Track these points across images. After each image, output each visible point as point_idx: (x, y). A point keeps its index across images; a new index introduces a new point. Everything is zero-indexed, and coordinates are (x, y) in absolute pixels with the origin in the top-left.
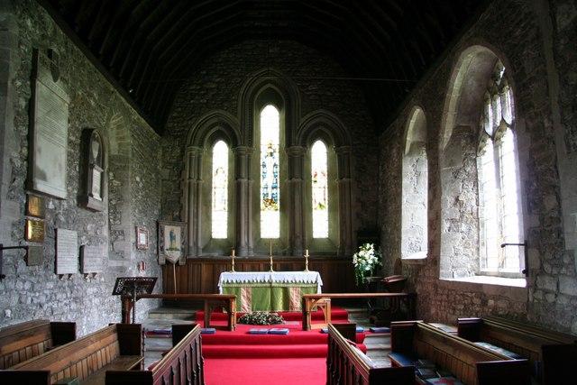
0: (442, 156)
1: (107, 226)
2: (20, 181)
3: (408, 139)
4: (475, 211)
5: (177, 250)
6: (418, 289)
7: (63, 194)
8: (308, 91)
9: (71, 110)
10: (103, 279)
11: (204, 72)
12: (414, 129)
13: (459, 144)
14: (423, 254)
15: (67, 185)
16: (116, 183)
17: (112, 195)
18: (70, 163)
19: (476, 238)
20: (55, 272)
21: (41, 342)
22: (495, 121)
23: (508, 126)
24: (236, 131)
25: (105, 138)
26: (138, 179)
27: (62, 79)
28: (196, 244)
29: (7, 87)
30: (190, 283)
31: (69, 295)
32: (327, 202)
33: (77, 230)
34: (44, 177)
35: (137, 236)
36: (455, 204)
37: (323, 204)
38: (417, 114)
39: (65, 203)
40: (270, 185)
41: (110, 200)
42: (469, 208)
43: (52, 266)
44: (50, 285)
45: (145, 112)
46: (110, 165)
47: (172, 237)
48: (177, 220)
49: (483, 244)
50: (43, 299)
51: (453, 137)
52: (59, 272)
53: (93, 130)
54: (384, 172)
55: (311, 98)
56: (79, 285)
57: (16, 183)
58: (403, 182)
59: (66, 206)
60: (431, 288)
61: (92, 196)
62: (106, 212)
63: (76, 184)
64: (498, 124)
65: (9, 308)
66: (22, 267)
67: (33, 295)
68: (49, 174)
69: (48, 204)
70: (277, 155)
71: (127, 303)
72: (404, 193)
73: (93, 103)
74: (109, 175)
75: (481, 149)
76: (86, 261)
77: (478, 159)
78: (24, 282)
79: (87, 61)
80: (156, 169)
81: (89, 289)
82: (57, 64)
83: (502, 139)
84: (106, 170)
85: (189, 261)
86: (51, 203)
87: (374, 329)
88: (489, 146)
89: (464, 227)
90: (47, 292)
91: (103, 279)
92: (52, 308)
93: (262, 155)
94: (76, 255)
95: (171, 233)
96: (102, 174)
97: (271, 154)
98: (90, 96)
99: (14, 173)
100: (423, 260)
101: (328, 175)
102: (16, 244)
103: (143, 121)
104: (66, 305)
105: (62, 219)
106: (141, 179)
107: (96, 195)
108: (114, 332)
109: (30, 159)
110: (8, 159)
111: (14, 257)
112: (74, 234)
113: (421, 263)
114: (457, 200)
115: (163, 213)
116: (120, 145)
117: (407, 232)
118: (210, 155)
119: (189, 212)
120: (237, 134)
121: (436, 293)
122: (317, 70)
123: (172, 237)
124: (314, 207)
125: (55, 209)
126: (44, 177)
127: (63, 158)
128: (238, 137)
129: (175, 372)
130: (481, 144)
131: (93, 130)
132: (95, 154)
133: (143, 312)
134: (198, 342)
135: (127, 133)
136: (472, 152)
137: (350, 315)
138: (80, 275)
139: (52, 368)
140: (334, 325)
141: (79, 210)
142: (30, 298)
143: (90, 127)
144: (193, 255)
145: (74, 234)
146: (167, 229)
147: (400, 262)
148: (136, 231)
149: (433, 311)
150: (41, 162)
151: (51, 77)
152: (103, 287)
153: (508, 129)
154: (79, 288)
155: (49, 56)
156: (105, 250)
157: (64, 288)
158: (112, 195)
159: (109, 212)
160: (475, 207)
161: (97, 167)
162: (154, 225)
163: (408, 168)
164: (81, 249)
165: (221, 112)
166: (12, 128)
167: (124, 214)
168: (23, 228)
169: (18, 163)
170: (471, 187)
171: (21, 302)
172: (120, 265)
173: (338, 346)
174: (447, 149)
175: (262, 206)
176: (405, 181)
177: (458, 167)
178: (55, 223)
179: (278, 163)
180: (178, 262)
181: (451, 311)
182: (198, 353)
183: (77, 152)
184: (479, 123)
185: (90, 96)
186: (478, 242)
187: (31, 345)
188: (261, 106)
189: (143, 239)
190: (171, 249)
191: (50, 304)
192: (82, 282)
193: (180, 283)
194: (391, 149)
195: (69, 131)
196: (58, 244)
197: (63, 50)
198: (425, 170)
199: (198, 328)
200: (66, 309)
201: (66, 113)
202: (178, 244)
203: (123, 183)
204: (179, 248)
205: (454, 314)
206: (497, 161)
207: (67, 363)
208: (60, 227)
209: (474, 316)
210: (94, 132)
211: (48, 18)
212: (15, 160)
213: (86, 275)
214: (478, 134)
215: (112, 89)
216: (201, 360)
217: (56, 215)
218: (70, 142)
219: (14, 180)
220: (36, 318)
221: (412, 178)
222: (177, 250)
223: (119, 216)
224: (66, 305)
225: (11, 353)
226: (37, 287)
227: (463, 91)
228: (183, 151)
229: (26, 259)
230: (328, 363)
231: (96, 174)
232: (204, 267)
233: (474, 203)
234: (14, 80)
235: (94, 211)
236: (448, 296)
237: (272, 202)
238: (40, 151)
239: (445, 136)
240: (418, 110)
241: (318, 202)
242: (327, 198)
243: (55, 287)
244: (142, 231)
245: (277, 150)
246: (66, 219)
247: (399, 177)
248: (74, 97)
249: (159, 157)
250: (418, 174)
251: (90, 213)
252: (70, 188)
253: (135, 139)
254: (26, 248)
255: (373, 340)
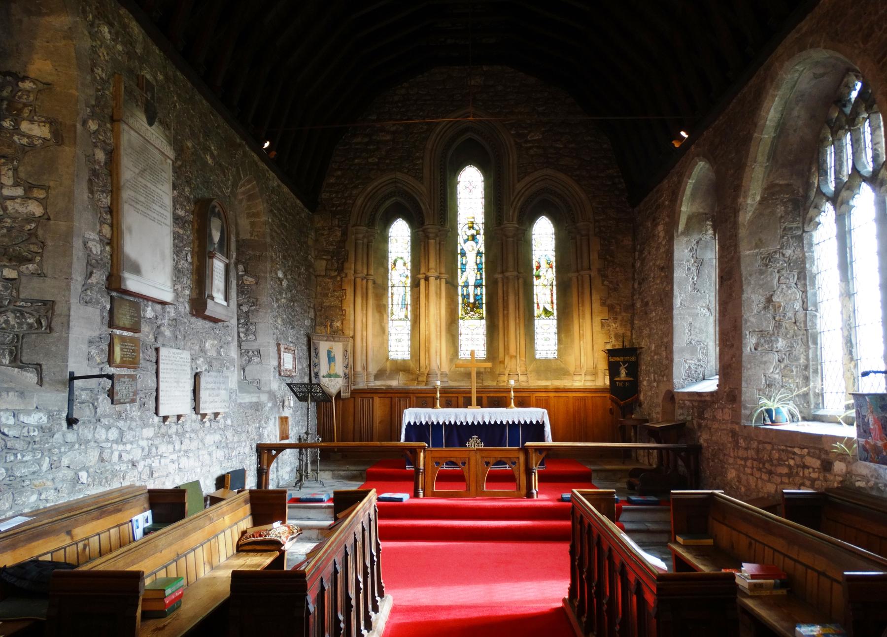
0: (743, 232)
1: (235, 343)
2: (99, 277)
3: (683, 209)
4: (801, 315)
5: (337, 376)
6: (703, 438)
7: (167, 296)
8: (527, 142)
9: (176, 170)
10: (229, 422)
11: (374, 117)
12: (693, 195)
13: (773, 213)
14: (710, 386)
15: (174, 283)
16: (249, 280)
17: (242, 299)
18: (177, 251)
19: (802, 361)
20: (157, 413)
21: (142, 519)
22: (838, 172)
23: (865, 179)
24: (422, 205)
25: (231, 214)
26: (280, 275)
27: (161, 123)
28: (365, 368)
29: (75, 132)
30: (365, 420)
31: (177, 447)
32: (555, 307)
33: (191, 349)
34: (136, 270)
35: (280, 358)
36: (766, 308)
37: (549, 308)
38: (700, 169)
39: (171, 310)
40: (472, 282)
41: (239, 306)
42: (790, 314)
43: (151, 404)
44: (149, 432)
45: (286, 177)
46: (237, 255)
47: (331, 359)
48: (335, 335)
49: (816, 371)
50: (137, 454)
51: (763, 200)
52: (162, 413)
53: (212, 200)
54: (643, 261)
55: (532, 152)
56: (193, 431)
57: (93, 280)
58: (675, 275)
59: (172, 314)
60: (726, 439)
61: (212, 298)
62: (234, 322)
63: (187, 281)
64: (845, 179)
65: (85, 468)
66: (103, 401)
67: (121, 447)
68: (145, 266)
69: (145, 311)
70: (481, 238)
71: (266, 456)
72: (676, 291)
73: (210, 161)
74: (237, 269)
75: (811, 220)
76: (204, 395)
77: (805, 236)
78: (108, 428)
79: (198, 97)
80: (306, 259)
81: (208, 437)
82: (152, 98)
83: (852, 203)
84: (233, 261)
85: (355, 393)
86: (149, 309)
87: (633, 498)
88: (827, 215)
89: (781, 344)
90: (144, 443)
91: (229, 422)
92: (150, 467)
93: (460, 240)
94: (189, 387)
95: (329, 352)
96: (227, 267)
97: (473, 238)
98: (207, 149)
99: (91, 265)
100: (711, 394)
101: (557, 267)
102: (96, 372)
103: (286, 189)
104: (173, 461)
105: (168, 333)
106: (285, 275)
107: (219, 297)
108: (246, 502)
109: (114, 242)
110: (80, 242)
111: (92, 391)
112: (186, 355)
113: (708, 398)
114: (769, 300)
115: (315, 322)
116: (253, 224)
117: (682, 350)
118: (385, 239)
119: (851, 502)
120: (423, 207)
121: (736, 446)
122: (541, 109)
123: (331, 359)
124: (536, 312)
125: (156, 318)
126: (136, 270)
127: (167, 242)
128: (424, 211)
129: (339, 568)
130: (812, 212)
131: (212, 200)
132: (216, 236)
133: (288, 469)
134: (372, 517)
135: (261, 206)
136: (794, 225)
137: (594, 475)
138: (194, 416)
139: (143, 566)
140: (583, 494)
141: (193, 319)
142: (116, 454)
143: (206, 195)
144: (361, 385)
145: (186, 355)
146: (324, 347)
147: (671, 396)
148: (279, 351)
149: (732, 474)
150: (131, 247)
151: (145, 120)
152: (229, 434)
153: (864, 185)
154: (193, 435)
155: (138, 85)
156: (233, 377)
157: (170, 437)
158: (242, 299)
159: (238, 324)
160: (801, 315)
161: (218, 255)
162: (305, 340)
163: (682, 252)
164: (197, 376)
165: (399, 176)
166: (86, 195)
167: (260, 326)
168: (105, 347)
169: (96, 248)
170: (793, 281)
171: (103, 460)
172: (255, 400)
173: (590, 526)
174: (751, 222)
175: (461, 312)
176: (679, 274)
177: (771, 249)
178: (156, 339)
179: (483, 250)
180: (339, 394)
181: (765, 477)
182: (373, 534)
183: (188, 234)
184: (809, 178)
185: (207, 149)
186: (806, 367)
187: (118, 526)
188: (458, 168)
189: (288, 362)
190: (329, 376)
191: (148, 461)
192: (197, 426)
193: (343, 422)
194: (656, 225)
195: (175, 201)
196: (161, 371)
197: (160, 77)
198: (711, 256)
199: (373, 495)
200: (172, 467)
201: (168, 175)
202: (339, 368)
203: (258, 279)
204: (342, 374)
205: (769, 481)
206: (843, 237)
207: (173, 555)
208: (164, 345)
209: (808, 488)
210: (214, 203)
211: (135, 29)
212: (90, 244)
213: (204, 416)
214: (806, 197)
215: (238, 141)
216: (378, 545)
217: (158, 327)
218: (176, 219)
219: (91, 273)
220: (126, 483)
221: (689, 269)
222: (337, 376)
223: (252, 328)
224: (173, 461)
225: (87, 539)
226: (128, 436)
227: (782, 128)
228: (345, 233)
229: (111, 393)
230: (572, 553)
231: (218, 266)
232: (377, 400)
233: (798, 306)
234: (84, 123)
235: (215, 320)
236: (758, 451)
237: (475, 306)
238: (130, 231)
239: (749, 201)
240: (701, 164)
241: (541, 308)
242: (555, 301)
243: (156, 435)
244: (287, 349)
245: (482, 232)
246: (174, 332)
247: (668, 269)
248: (180, 150)
249: (310, 243)
250: (700, 264)
251: (208, 324)
252: (179, 287)
253: (274, 215)
254: (110, 377)
255: (637, 516)
